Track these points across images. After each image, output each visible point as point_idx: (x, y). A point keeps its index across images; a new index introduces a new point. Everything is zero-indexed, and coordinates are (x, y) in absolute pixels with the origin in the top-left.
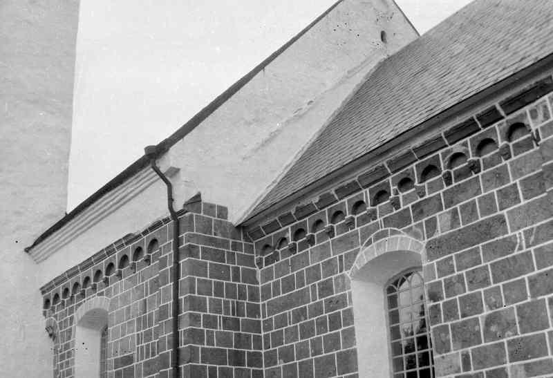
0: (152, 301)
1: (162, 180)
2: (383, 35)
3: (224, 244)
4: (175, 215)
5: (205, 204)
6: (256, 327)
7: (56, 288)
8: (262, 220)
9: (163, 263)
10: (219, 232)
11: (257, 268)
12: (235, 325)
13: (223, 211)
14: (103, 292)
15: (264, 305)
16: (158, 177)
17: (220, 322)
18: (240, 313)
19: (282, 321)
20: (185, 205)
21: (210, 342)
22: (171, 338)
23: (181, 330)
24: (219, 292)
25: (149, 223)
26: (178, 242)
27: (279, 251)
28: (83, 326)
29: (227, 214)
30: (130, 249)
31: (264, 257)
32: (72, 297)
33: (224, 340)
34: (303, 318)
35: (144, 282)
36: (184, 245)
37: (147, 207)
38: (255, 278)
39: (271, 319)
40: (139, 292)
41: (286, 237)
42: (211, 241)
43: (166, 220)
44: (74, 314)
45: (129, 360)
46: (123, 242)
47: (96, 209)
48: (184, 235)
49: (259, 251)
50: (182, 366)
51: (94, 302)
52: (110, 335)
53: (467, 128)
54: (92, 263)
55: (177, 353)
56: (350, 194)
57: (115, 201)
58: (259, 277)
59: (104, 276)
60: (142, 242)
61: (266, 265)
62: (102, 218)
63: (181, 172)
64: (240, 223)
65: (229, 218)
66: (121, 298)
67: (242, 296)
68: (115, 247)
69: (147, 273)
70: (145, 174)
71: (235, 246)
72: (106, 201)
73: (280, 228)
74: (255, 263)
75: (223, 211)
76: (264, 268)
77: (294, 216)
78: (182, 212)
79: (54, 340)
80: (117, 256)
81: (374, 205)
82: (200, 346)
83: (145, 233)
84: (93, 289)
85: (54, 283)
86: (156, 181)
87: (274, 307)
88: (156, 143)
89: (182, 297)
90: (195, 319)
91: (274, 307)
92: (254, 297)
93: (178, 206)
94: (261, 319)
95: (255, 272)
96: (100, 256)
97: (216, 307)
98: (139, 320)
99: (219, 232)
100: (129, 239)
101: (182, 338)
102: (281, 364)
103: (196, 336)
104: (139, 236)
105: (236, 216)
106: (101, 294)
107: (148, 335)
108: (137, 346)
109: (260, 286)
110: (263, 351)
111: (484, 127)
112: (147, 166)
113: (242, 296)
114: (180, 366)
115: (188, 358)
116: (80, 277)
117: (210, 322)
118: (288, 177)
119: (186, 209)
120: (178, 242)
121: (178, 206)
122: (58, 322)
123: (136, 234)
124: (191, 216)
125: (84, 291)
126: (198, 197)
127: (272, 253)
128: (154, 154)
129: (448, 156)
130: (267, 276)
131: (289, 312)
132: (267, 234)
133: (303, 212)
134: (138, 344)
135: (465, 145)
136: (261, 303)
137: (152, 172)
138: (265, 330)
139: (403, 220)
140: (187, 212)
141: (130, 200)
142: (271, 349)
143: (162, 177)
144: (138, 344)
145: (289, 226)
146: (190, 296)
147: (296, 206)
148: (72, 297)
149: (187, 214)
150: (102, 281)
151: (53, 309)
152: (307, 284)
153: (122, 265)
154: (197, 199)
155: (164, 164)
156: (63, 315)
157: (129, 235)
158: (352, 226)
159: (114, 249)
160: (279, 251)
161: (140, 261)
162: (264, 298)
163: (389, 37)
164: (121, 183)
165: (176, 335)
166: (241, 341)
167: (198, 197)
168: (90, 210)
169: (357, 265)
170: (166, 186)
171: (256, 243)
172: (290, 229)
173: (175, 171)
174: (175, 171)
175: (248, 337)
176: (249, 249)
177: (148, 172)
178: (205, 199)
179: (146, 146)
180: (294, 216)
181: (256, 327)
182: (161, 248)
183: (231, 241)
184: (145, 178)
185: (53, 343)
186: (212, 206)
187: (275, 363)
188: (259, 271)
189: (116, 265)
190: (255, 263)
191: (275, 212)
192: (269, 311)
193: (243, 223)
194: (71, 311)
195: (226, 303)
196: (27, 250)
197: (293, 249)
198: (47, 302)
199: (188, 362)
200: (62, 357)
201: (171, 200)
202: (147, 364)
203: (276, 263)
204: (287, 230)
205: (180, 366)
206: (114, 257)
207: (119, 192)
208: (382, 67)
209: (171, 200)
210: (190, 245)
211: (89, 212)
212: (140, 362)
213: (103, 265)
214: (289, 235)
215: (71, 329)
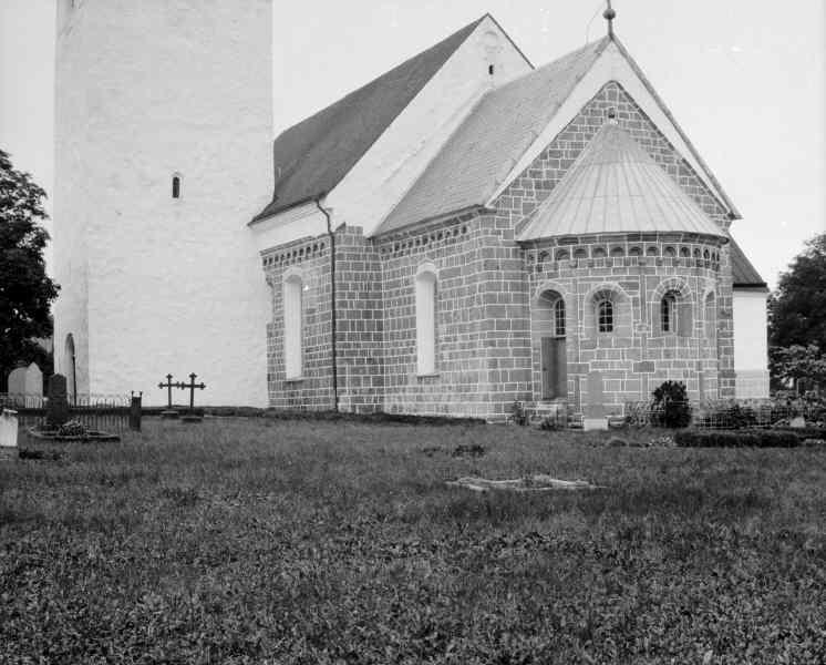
2: (491, 68)
3: (360, 250)
12: (367, 296)
13: (359, 230)
21: (351, 306)
26: (334, 251)
33: (359, 305)
45: (313, 311)
51: (293, 270)
53: (449, 223)
66: (310, 272)
75: (359, 230)
97: (355, 288)
101: (337, 305)
103: (343, 304)
105: (367, 233)
117: (351, 296)
118: (389, 217)
120: (334, 251)
130: (385, 267)
133: (398, 237)
135: (450, 229)
139: (432, 256)
143: (324, 212)
163: (495, 70)
165: (333, 303)
166: (370, 305)
169: (418, 273)
173: (330, 210)
176: (376, 250)
177: (312, 207)
178: (348, 224)
181: (380, 296)
186: (353, 227)
196: (249, 225)
198: (265, 262)
201: (329, 226)
208: (488, 96)
209: (329, 226)
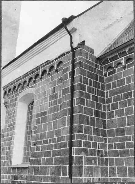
0: (58, 87)
1: (68, 34)
4: (73, 49)
5: (86, 46)
6: (103, 101)
7: (46, 66)
8: (107, 56)
9: (65, 71)
10: (91, 58)
11: (104, 77)
14: (32, 86)
15: (107, 93)
16: (67, 33)
17: (91, 97)
18: (98, 94)
19: (118, 99)
20: (78, 45)
22: (133, 76)
23: (75, 98)
24: (90, 84)
25: (59, 55)
27: (116, 69)
28: (21, 101)
29: (94, 52)
30: (47, 68)
31: (108, 72)
32: (17, 90)
34: (129, 97)
35: (54, 80)
36: (77, 62)
37: (61, 45)
38: (103, 80)
39: (111, 98)
40: (51, 85)
41: (121, 62)
42: (88, 61)
43: (68, 53)
44: (18, 97)
45: (45, 113)
46: (45, 64)
47: (35, 49)
48: (77, 58)
49: (106, 69)
50: (75, 115)
51: (28, 90)
52: (69, 90)
54: (44, 65)
55: (72, 108)
56: (125, 56)
57: (42, 47)
58: (105, 81)
59: (34, 80)
60: (54, 64)
61: (108, 76)
62: (43, 50)
63: (77, 31)
64: (99, 56)
65: (94, 53)
67: (99, 87)
68: (40, 66)
69: (55, 77)
70: (59, 33)
71: (97, 66)
72: (38, 47)
73: (118, 58)
74: (104, 74)
75: (92, 51)
76: (107, 77)
77: (127, 52)
78: (77, 48)
79: (6, 108)
80: (41, 70)
81: (126, 63)
82: (83, 106)
83: (56, 59)
84: (28, 85)
85: (15, 81)
86: (66, 35)
87: (113, 93)
88: (67, 17)
89: (75, 84)
90: (81, 94)
91: (113, 93)
92: (103, 89)
93: (75, 45)
94: (106, 98)
95: (103, 78)
96: (32, 71)
98: (50, 96)
99: (91, 58)
100: (47, 62)
101: (75, 102)
102: (116, 117)
104: (53, 61)
105: (97, 54)
106: (32, 87)
107: (55, 102)
108: (48, 108)
109: (105, 84)
110: (106, 112)
111: (129, 54)
112: (63, 27)
113: (99, 87)
114: (73, 115)
115: (78, 110)
116: (22, 80)
119: (79, 46)
121: (75, 45)
122: (9, 100)
123: (52, 60)
124: (81, 50)
125: (23, 87)
126: (84, 42)
127: (113, 70)
128: (66, 22)
129: (117, 63)
131: (122, 95)
132: (111, 62)
134: (49, 106)
136: (105, 91)
137: (65, 31)
138: (107, 103)
140: (79, 47)
141: (49, 46)
142: (111, 111)
144: (49, 106)
145: (123, 58)
146: (80, 83)
147: (129, 48)
148: (17, 90)
149: (79, 49)
150: (26, 85)
151: (8, 96)
152: (67, 109)
153: (43, 74)
154: (83, 43)
155: (69, 27)
156: (13, 97)
157: (48, 61)
158: (125, 68)
159: (40, 68)
160: (116, 69)
161: (52, 72)
162: (107, 89)
164: (46, 38)
167: (84, 42)
168: (30, 52)
170: (69, 37)
171: (104, 66)
172: (124, 59)
173: (74, 30)
174: (74, 30)
175: (101, 105)
177: (63, 30)
179: (62, 18)
180: (127, 52)
182: (64, 65)
183: (95, 63)
184: (58, 35)
185: (6, 109)
186: (88, 48)
187: (113, 117)
188: (105, 78)
189: (12, 89)
190: (104, 74)
191: (117, 51)
192: (110, 94)
193: (99, 57)
194: (16, 95)
195: (93, 89)
197: (125, 67)
199: (78, 113)
200: (11, 114)
201: (72, 43)
202: (54, 115)
203: (114, 74)
204: (122, 59)
205: (73, 115)
206: (39, 71)
207: (44, 43)
209: (72, 43)
210: (80, 61)
211: (29, 53)
212: (50, 114)
213: (33, 75)
214: (123, 62)
215: (16, 103)
